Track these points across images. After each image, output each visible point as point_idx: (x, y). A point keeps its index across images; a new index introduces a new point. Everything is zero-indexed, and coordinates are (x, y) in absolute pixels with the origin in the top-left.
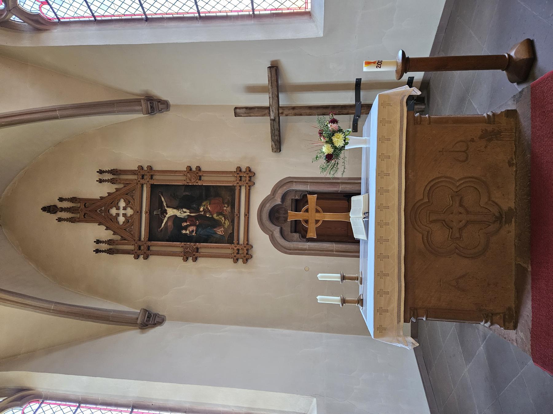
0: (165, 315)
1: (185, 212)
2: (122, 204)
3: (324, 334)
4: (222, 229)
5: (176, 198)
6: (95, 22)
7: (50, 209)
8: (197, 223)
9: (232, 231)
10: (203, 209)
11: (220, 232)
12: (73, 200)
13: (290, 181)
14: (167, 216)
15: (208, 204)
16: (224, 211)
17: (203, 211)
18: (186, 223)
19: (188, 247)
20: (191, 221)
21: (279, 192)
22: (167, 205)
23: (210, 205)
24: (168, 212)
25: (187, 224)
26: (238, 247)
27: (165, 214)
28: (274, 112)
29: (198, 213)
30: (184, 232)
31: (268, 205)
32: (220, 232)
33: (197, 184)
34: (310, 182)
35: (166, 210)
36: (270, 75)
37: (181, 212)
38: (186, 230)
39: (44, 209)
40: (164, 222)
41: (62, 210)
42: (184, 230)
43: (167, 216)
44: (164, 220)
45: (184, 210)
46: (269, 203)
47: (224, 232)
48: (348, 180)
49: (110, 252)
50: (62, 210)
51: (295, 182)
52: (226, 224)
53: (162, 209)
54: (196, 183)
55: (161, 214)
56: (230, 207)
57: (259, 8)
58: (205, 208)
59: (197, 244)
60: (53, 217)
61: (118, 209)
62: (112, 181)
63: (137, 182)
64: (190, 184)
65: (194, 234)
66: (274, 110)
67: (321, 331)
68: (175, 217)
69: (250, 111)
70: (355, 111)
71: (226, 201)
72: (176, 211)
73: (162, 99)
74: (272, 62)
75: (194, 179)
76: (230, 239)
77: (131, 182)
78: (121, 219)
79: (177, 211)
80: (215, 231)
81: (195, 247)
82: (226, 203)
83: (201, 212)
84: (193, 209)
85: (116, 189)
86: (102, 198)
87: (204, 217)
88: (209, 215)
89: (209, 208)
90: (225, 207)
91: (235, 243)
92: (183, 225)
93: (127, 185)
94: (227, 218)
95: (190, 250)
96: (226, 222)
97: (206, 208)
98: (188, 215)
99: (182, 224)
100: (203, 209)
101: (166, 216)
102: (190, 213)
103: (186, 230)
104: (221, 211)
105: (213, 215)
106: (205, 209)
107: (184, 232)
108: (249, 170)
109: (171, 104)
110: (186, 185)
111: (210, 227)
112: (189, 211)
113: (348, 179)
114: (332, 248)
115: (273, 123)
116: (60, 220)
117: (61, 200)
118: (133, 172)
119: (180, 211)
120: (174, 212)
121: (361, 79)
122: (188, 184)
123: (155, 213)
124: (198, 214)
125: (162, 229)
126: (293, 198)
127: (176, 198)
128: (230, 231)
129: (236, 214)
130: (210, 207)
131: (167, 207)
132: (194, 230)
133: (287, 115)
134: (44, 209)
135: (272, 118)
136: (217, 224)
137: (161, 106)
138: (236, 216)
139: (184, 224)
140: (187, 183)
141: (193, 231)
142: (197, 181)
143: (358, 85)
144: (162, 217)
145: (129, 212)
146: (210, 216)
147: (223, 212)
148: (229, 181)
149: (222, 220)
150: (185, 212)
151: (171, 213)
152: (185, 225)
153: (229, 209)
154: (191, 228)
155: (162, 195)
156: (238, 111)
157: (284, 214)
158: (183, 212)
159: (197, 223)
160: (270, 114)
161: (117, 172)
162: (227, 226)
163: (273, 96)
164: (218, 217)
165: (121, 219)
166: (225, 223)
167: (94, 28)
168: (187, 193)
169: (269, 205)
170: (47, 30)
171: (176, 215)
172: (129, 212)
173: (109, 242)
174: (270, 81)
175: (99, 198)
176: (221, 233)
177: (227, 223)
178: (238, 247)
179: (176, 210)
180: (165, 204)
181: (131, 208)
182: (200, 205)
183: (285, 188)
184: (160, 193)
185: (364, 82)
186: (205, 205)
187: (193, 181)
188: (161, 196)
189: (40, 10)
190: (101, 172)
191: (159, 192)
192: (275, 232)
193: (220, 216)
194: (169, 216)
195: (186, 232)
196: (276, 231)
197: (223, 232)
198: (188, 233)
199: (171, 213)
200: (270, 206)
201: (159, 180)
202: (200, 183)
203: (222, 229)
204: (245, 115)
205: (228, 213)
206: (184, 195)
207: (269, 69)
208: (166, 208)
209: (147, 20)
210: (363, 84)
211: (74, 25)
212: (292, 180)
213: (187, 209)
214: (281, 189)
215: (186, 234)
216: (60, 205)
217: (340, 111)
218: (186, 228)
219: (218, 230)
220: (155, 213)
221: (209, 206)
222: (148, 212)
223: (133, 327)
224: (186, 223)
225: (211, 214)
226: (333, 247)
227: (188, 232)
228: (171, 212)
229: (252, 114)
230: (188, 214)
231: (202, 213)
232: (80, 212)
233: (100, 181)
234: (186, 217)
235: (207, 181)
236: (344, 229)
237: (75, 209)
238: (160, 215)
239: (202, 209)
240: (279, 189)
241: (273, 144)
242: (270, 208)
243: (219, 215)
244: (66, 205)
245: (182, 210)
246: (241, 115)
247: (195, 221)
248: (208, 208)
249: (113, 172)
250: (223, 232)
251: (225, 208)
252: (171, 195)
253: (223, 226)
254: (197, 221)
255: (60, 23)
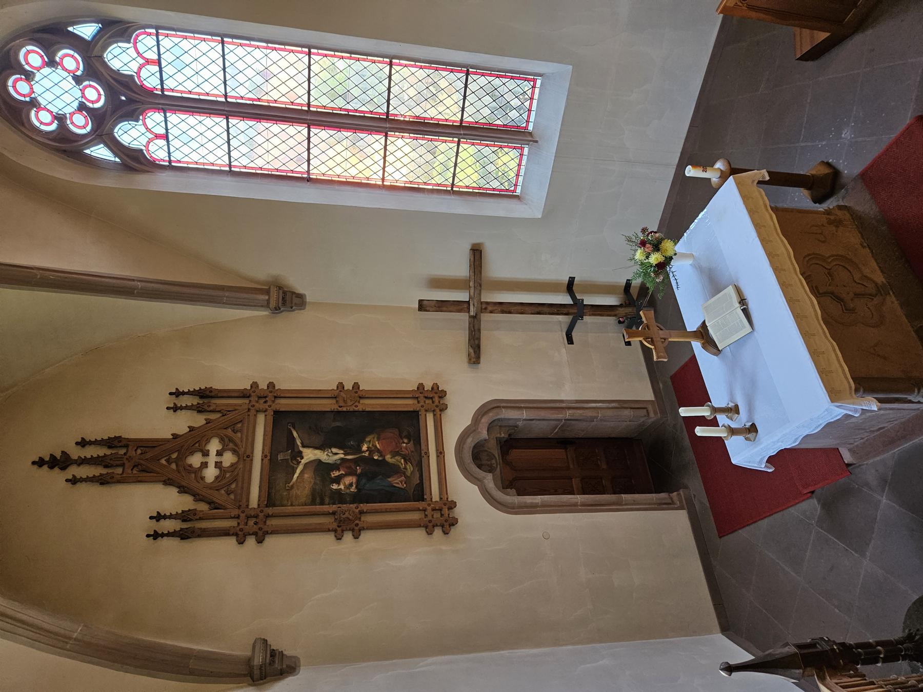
0: (299, 656)
1: (336, 454)
2: (214, 446)
3: (598, 645)
4: (403, 478)
5: (320, 432)
6: (229, 173)
7: (58, 462)
8: (359, 471)
9: (419, 482)
10: (367, 448)
11: (399, 484)
12: (112, 442)
13: (496, 405)
14: (303, 461)
15: (376, 439)
16: (403, 449)
17: (367, 451)
18: (338, 472)
19: (346, 511)
20: (346, 467)
21: (483, 420)
22: (302, 443)
23: (378, 439)
24: (304, 454)
25: (341, 473)
26: (433, 506)
27: (299, 459)
28: (476, 306)
29: (360, 453)
30: (335, 487)
31: (469, 440)
32: (399, 484)
33: (356, 409)
34: (524, 407)
35: (301, 452)
36: (472, 259)
37: (329, 454)
38: (339, 484)
39: (40, 463)
40: (298, 471)
41: (82, 462)
42: (334, 484)
43: (303, 461)
44: (297, 468)
45: (334, 450)
46: (470, 437)
47: (405, 483)
48: (575, 403)
49: (183, 535)
50: (82, 462)
51: (504, 407)
52: (409, 470)
53: (293, 450)
54: (355, 406)
55: (291, 459)
56: (412, 442)
57: (461, 184)
58: (371, 446)
59: (361, 505)
60: (58, 477)
61: (206, 454)
62: (200, 410)
63: (250, 407)
64: (345, 409)
65: (353, 489)
66: (476, 304)
67: (592, 641)
68: (319, 462)
69: (441, 306)
70: (576, 311)
71: (405, 434)
72: (319, 453)
73: (297, 292)
74: (479, 245)
75: (351, 401)
76: (419, 493)
77: (236, 408)
78: (211, 473)
79: (322, 453)
80: (390, 482)
81: (357, 511)
82: (406, 437)
83: (364, 452)
84: (350, 448)
85: (206, 420)
86: (175, 436)
87: (370, 460)
88: (379, 457)
89: (378, 446)
90: (404, 443)
91: (428, 500)
92: (333, 475)
93: (228, 413)
94: (410, 459)
95: (350, 515)
96: (408, 467)
97: (373, 445)
98: (342, 459)
99: (332, 473)
100: (367, 448)
101: (300, 462)
102: (345, 454)
103: (339, 484)
104: (397, 450)
105: (385, 456)
106: (371, 448)
107: (335, 487)
108: (435, 387)
109: (307, 300)
110: (339, 412)
111: (381, 477)
112: (342, 452)
113: (575, 402)
114: (576, 500)
115: (473, 321)
116: (74, 481)
117: (83, 443)
118: (243, 394)
119: (326, 453)
120: (315, 455)
121: (575, 277)
122: (340, 409)
123: (280, 457)
124: (357, 456)
125: (293, 484)
126: (499, 435)
127: (320, 432)
128: (416, 481)
129: (424, 451)
130: (378, 443)
131: (304, 446)
132: (352, 483)
133: (491, 312)
134: (40, 463)
135: (472, 313)
136: (395, 470)
137: (296, 300)
138: (425, 456)
139: (335, 474)
140: (339, 407)
141: (351, 485)
142: (357, 404)
143: (570, 286)
144: (293, 463)
145: (228, 459)
146: (380, 459)
147: (401, 451)
148: (408, 405)
149: (400, 464)
150: (336, 454)
151: (310, 456)
152: (335, 475)
153: (411, 445)
154: (348, 480)
155: (294, 428)
156: (423, 306)
157: (487, 460)
158: (333, 453)
159: (359, 471)
160: (469, 309)
161: (211, 392)
162: (409, 472)
163: (476, 286)
164: (394, 460)
165: (211, 473)
166: (405, 468)
167: (229, 179)
168: (338, 424)
169: (471, 441)
170: (148, 172)
171: (320, 460)
172: (228, 459)
173: (184, 516)
174: (473, 266)
175: (171, 437)
176: (400, 486)
177: (410, 468)
178: (433, 506)
179: (320, 451)
180: (299, 442)
181: (234, 452)
182: (361, 441)
183: (491, 414)
184: (290, 424)
185: (578, 283)
186: (370, 441)
187: (349, 403)
188: (292, 429)
189: (147, 146)
190: (177, 394)
191: (288, 423)
192: (486, 481)
193: (397, 458)
194: (307, 461)
195: (338, 486)
196: (489, 480)
197: (403, 483)
198: (343, 489)
199: (310, 456)
200: (472, 441)
201: (284, 404)
202: (360, 408)
203: (403, 478)
204: (433, 309)
205: (409, 451)
206: (333, 427)
207: (471, 251)
208: (301, 449)
209: (309, 180)
210: (577, 284)
211: (193, 172)
212: (498, 405)
213: (340, 448)
214: (486, 416)
215: (339, 491)
216: (76, 453)
217: (559, 309)
218: (338, 480)
219: (395, 480)
220: (280, 457)
221: (377, 442)
222: (269, 455)
223: (235, 685)
224: (338, 472)
225: (381, 456)
226: (577, 498)
227: (342, 487)
228: (311, 455)
229: (444, 309)
230: (342, 456)
231: (367, 454)
232: (126, 462)
233: (175, 409)
234: (339, 462)
235: (368, 405)
236: (568, 491)
237: (115, 458)
238: (290, 461)
239: (365, 448)
240: (481, 418)
241: (472, 351)
242: (473, 445)
243: (396, 456)
244: (91, 452)
245: (330, 451)
246: (428, 309)
247: (353, 467)
248: (376, 446)
249: (205, 394)
250: (403, 483)
251: (405, 445)
252: (310, 428)
253: (404, 473)
254: (358, 468)
255: (170, 167)
